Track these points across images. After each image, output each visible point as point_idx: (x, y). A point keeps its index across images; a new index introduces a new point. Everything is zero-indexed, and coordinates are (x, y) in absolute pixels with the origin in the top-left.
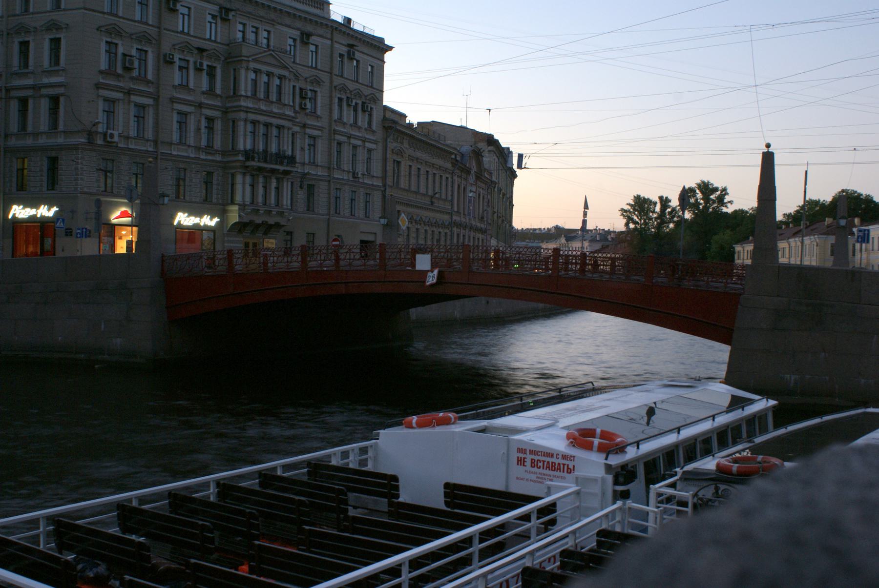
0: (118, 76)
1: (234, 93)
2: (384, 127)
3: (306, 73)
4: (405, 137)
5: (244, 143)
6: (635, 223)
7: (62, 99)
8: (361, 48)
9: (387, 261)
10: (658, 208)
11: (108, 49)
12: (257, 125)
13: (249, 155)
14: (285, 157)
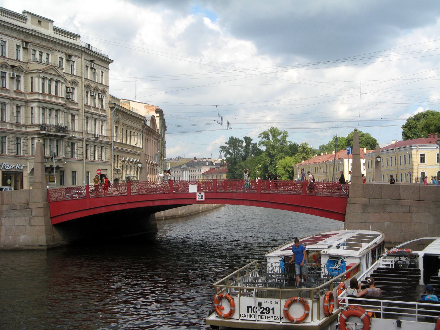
1: (32, 91)
2: (110, 107)
3: (69, 78)
4: (120, 112)
6: (230, 154)
8: (97, 62)
9: (131, 190)
10: (244, 144)
11: (43, 82)
12: (45, 109)
13: (42, 127)
14: (61, 128)
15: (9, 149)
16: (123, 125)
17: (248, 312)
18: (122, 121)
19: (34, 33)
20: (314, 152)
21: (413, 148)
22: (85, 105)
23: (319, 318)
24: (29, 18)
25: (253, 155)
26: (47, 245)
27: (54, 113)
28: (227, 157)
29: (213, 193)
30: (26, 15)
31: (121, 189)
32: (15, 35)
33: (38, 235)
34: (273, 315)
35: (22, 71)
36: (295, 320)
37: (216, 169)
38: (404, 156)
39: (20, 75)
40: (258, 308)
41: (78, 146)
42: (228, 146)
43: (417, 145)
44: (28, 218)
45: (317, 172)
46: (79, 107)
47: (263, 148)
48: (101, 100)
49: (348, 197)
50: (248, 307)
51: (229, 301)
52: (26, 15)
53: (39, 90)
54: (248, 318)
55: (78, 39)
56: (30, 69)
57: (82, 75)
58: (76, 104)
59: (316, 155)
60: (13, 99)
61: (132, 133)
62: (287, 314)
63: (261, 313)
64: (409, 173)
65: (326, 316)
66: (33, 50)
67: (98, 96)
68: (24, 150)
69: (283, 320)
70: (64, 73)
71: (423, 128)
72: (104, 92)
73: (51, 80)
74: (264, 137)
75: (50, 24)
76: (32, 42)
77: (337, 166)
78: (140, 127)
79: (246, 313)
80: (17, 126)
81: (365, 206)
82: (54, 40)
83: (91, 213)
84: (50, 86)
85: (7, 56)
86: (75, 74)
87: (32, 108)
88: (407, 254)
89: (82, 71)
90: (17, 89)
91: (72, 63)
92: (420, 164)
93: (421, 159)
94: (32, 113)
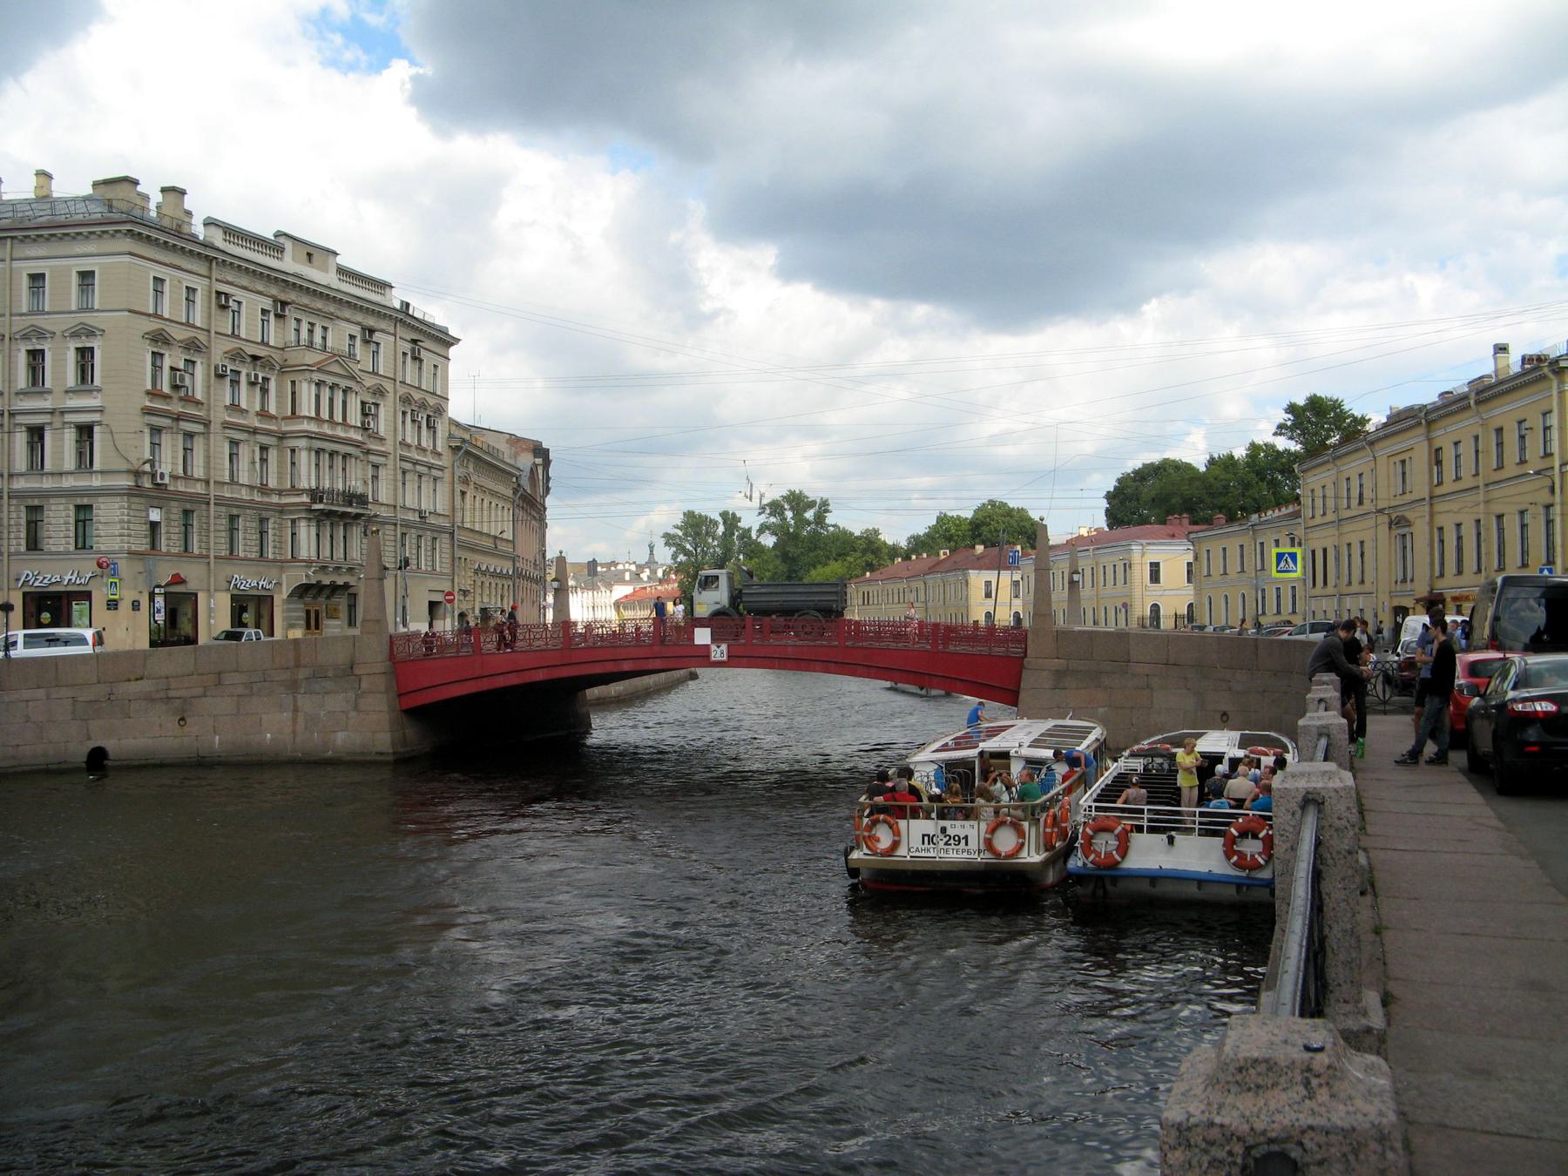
0: (166, 397)
1: (293, 412)
3: (370, 382)
5: (306, 480)
6: (686, 553)
7: (96, 429)
8: (427, 344)
10: (721, 529)
12: (335, 456)
13: (316, 495)
15: (246, 545)
16: (478, 487)
17: (923, 843)
18: (474, 478)
19: (299, 282)
20: (894, 551)
21: (1133, 547)
22: (400, 443)
23: (1038, 854)
24: (288, 245)
25: (741, 557)
26: (394, 753)
27: (339, 461)
28: (679, 560)
29: (744, 645)
30: (282, 240)
31: (532, 637)
32: (260, 288)
33: (373, 732)
34: (966, 848)
35: (272, 368)
36: (1003, 854)
37: (648, 589)
38: (1112, 568)
39: (268, 376)
40: (941, 836)
41: (386, 537)
42: (680, 533)
43: (1144, 542)
44: (351, 695)
45: (901, 601)
46: (388, 447)
47: (769, 541)
48: (431, 427)
49: (1026, 656)
50: (924, 836)
51: (891, 828)
52: (282, 240)
53: (309, 412)
54: (923, 854)
55: (387, 290)
56: (290, 362)
57: (395, 374)
58: (382, 439)
59: (900, 560)
60: (255, 431)
61: (493, 505)
62: (989, 844)
63: (946, 844)
64: (1125, 605)
65: (1046, 850)
66: (295, 319)
67: (427, 420)
68: (275, 547)
69: (982, 854)
70: (360, 370)
71: (1153, 500)
72: (440, 411)
73: (333, 387)
74: (770, 514)
75: (331, 257)
76: (293, 302)
77: (953, 586)
78: (509, 493)
79: (920, 846)
80: (262, 493)
81: (1059, 675)
82: (339, 296)
83: (484, 685)
84: (331, 400)
85: (243, 335)
86: (381, 372)
87: (293, 451)
88: (1165, 753)
89: (395, 365)
90: (419, 444)
91: (373, 347)
92: (1149, 584)
93: (1151, 575)
94: (293, 464)
